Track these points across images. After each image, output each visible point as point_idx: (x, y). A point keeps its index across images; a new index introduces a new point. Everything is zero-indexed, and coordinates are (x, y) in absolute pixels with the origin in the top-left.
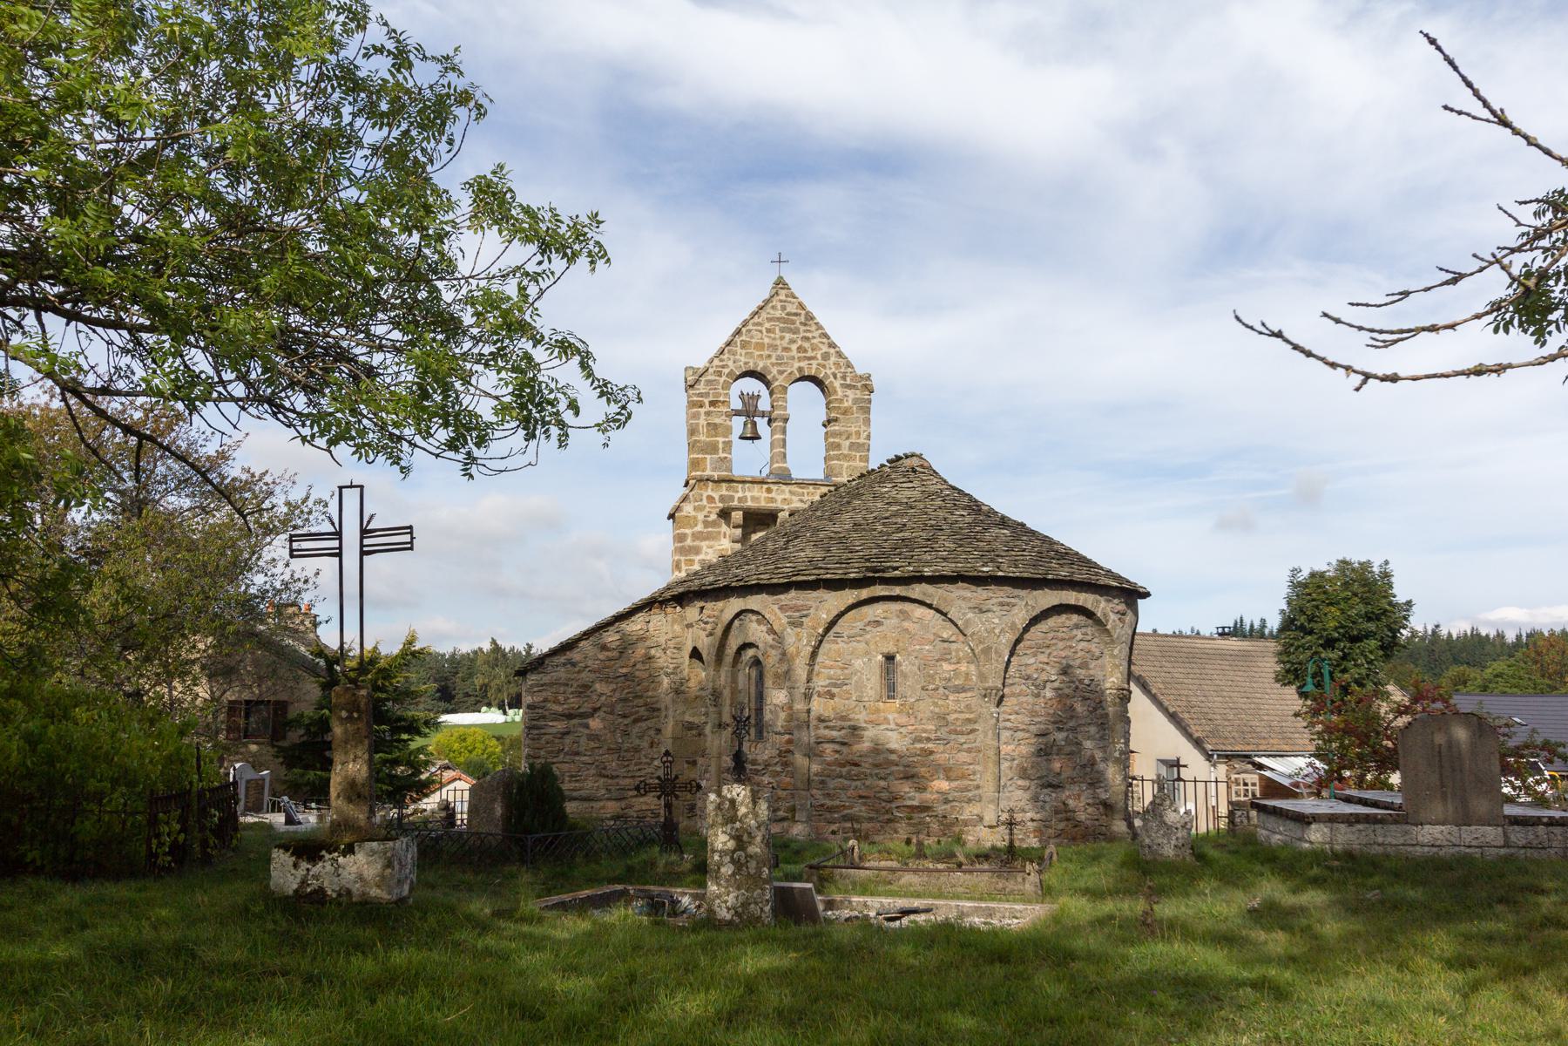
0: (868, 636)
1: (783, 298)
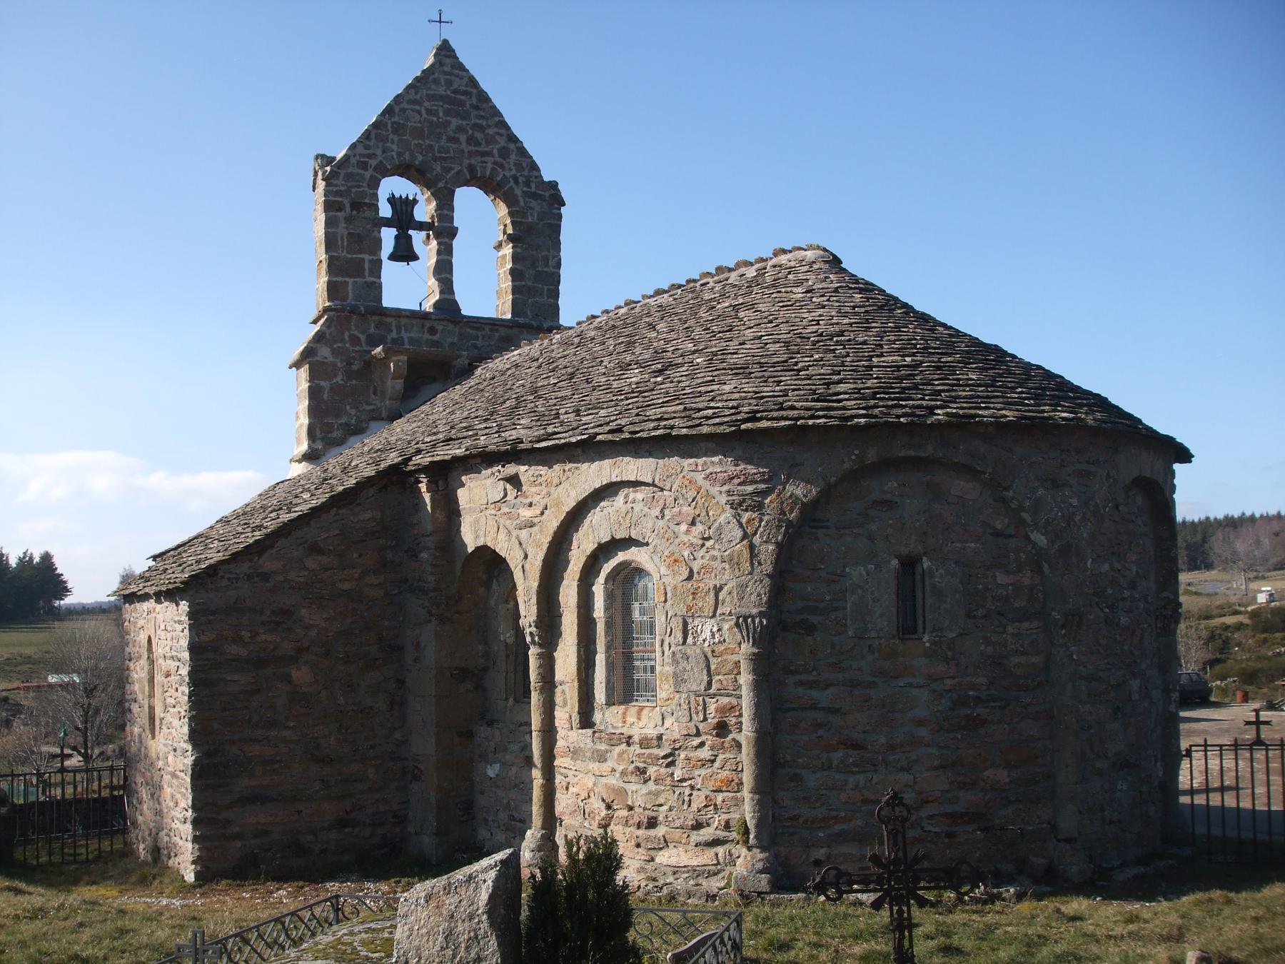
0: (873, 527)
1: (447, 69)
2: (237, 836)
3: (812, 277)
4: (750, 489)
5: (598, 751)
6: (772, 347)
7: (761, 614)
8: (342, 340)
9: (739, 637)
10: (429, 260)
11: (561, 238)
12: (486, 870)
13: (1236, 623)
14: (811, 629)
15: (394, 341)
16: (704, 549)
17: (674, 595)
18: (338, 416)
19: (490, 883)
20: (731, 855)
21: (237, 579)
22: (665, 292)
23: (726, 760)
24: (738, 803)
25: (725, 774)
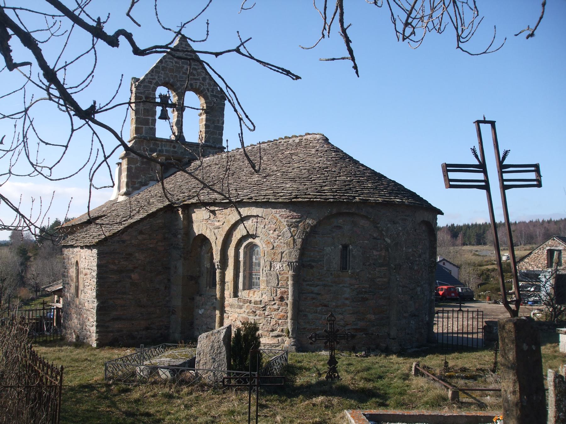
0: (334, 234)
1: (184, 46)
2: (112, 332)
3: (318, 145)
4: (294, 220)
5: (239, 305)
6: (303, 171)
7: (296, 262)
8: (140, 150)
9: (289, 269)
10: (174, 119)
11: (225, 113)
12: (223, 329)
13: (492, 269)
14: (312, 267)
15: (160, 151)
16: (278, 239)
17: (268, 254)
18: (138, 178)
19: (224, 333)
20: (283, 340)
21: (114, 242)
22: (266, 143)
23: (283, 309)
24: (286, 323)
25: (282, 314)
